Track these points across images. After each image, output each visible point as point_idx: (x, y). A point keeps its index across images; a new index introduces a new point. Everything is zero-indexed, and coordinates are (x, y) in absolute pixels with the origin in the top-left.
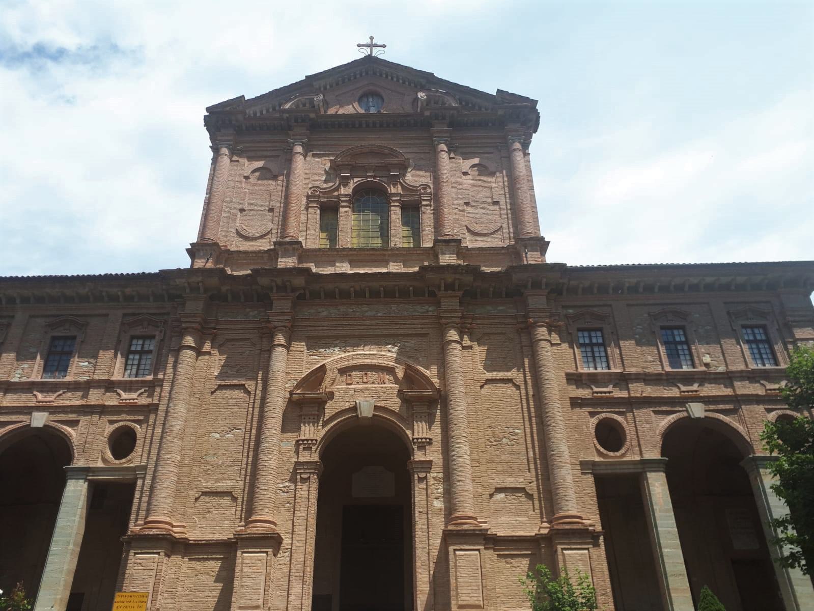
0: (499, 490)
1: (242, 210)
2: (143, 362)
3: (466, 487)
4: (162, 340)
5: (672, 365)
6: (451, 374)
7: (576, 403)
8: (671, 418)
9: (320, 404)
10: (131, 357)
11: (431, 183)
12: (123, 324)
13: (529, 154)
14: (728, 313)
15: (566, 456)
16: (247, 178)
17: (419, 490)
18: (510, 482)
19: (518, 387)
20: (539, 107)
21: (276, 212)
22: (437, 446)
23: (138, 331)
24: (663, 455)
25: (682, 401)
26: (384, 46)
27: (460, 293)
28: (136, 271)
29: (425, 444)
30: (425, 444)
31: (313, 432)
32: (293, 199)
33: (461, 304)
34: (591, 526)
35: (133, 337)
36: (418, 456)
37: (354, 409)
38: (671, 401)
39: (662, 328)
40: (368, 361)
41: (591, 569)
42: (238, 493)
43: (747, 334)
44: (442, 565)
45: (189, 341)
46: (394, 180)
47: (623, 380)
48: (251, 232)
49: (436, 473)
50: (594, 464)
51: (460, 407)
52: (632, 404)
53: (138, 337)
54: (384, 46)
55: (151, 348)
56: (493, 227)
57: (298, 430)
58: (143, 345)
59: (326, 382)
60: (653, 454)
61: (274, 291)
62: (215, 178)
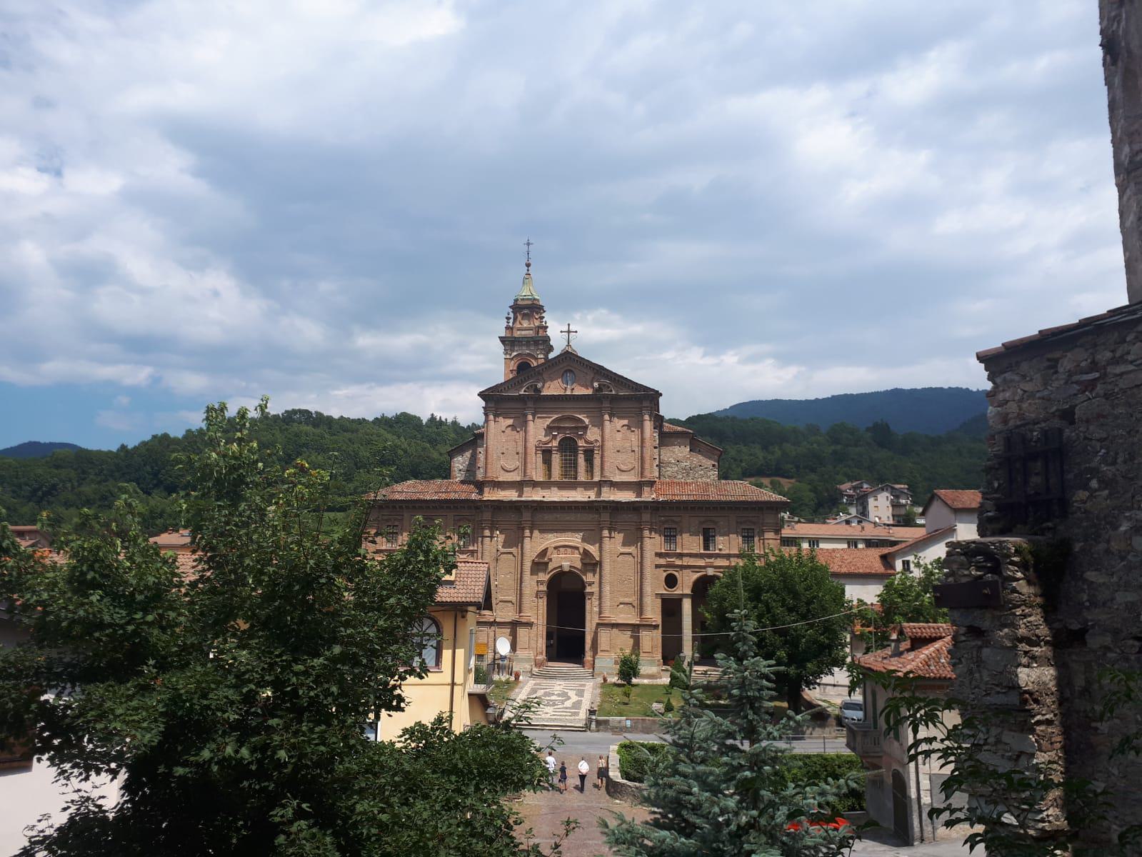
0: (621, 603)
1: (503, 453)
3: (607, 603)
5: (705, 549)
6: (604, 553)
7: (657, 566)
8: (699, 574)
9: (547, 564)
11: (599, 439)
15: (649, 593)
16: (503, 432)
17: (588, 603)
18: (627, 600)
19: (634, 557)
20: (661, 399)
21: (520, 455)
22: (596, 585)
25: (705, 567)
29: (591, 584)
30: (591, 584)
31: (544, 577)
32: (529, 451)
36: (588, 589)
37: (561, 567)
38: (700, 567)
40: (567, 543)
42: (514, 601)
44: (596, 633)
45: (487, 533)
46: (581, 437)
47: (681, 556)
48: (508, 467)
49: (596, 596)
50: (662, 594)
51: (607, 567)
52: (683, 567)
54: (576, 332)
56: (630, 466)
57: (537, 575)
59: (548, 553)
60: (688, 591)
62: (489, 466)
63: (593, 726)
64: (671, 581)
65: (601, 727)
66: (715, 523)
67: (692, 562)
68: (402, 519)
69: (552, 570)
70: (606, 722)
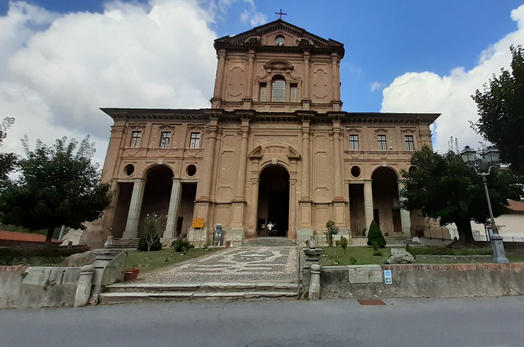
2: (196, 142)
4: (203, 135)
8: (377, 166)
10: (192, 140)
12: (188, 128)
13: (339, 66)
14: (401, 131)
20: (344, 47)
23: (194, 131)
24: (372, 178)
26: (286, 14)
27: (310, 121)
28: (113, 107)
33: (310, 124)
34: (345, 200)
35: (192, 133)
38: (377, 161)
39: (405, 136)
41: (295, 210)
43: (406, 139)
53: (194, 133)
54: (286, 14)
55: (199, 137)
58: (196, 136)
61: (303, 119)
63: (315, 285)
64: (356, 171)
65: (332, 287)
66: (386, 131)
67: (371, 157)
68: (145, 127)
69: (263, 164)
70: (342, 276)
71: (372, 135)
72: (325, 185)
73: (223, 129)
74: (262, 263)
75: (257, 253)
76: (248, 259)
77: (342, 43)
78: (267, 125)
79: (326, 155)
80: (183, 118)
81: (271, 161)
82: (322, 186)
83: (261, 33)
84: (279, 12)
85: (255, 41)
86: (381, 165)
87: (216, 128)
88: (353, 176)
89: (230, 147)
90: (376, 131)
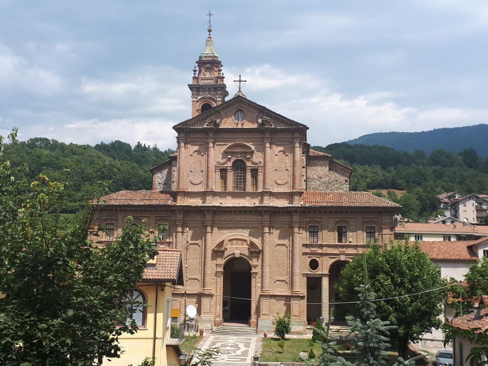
8: (334, 260)
64: (314, 265)
66: (347, 222)
68: (117, 219)
71: (333, 226)
72: (285, 278)
73: (187, 221)
74: (235, 356)
75: (228, 346)
76: (226, 352)
77: (304, 124)
78: (229, 216)
79: (286, 248)
80: (151, 211)
81: (234, 254)
82: (281, 278)
83: (219, 111)
84: (238, 79)
85: (214, 122)
86: (339, 259)
87: (182, 222)
88: (310, 269)
89: (195, 238)
90: (337, 223)
